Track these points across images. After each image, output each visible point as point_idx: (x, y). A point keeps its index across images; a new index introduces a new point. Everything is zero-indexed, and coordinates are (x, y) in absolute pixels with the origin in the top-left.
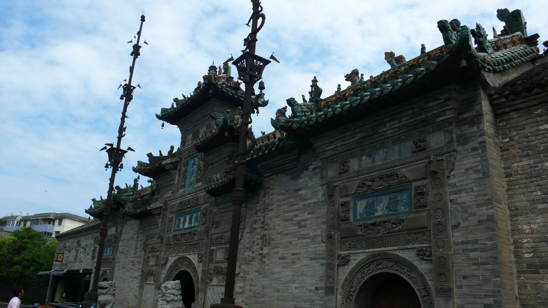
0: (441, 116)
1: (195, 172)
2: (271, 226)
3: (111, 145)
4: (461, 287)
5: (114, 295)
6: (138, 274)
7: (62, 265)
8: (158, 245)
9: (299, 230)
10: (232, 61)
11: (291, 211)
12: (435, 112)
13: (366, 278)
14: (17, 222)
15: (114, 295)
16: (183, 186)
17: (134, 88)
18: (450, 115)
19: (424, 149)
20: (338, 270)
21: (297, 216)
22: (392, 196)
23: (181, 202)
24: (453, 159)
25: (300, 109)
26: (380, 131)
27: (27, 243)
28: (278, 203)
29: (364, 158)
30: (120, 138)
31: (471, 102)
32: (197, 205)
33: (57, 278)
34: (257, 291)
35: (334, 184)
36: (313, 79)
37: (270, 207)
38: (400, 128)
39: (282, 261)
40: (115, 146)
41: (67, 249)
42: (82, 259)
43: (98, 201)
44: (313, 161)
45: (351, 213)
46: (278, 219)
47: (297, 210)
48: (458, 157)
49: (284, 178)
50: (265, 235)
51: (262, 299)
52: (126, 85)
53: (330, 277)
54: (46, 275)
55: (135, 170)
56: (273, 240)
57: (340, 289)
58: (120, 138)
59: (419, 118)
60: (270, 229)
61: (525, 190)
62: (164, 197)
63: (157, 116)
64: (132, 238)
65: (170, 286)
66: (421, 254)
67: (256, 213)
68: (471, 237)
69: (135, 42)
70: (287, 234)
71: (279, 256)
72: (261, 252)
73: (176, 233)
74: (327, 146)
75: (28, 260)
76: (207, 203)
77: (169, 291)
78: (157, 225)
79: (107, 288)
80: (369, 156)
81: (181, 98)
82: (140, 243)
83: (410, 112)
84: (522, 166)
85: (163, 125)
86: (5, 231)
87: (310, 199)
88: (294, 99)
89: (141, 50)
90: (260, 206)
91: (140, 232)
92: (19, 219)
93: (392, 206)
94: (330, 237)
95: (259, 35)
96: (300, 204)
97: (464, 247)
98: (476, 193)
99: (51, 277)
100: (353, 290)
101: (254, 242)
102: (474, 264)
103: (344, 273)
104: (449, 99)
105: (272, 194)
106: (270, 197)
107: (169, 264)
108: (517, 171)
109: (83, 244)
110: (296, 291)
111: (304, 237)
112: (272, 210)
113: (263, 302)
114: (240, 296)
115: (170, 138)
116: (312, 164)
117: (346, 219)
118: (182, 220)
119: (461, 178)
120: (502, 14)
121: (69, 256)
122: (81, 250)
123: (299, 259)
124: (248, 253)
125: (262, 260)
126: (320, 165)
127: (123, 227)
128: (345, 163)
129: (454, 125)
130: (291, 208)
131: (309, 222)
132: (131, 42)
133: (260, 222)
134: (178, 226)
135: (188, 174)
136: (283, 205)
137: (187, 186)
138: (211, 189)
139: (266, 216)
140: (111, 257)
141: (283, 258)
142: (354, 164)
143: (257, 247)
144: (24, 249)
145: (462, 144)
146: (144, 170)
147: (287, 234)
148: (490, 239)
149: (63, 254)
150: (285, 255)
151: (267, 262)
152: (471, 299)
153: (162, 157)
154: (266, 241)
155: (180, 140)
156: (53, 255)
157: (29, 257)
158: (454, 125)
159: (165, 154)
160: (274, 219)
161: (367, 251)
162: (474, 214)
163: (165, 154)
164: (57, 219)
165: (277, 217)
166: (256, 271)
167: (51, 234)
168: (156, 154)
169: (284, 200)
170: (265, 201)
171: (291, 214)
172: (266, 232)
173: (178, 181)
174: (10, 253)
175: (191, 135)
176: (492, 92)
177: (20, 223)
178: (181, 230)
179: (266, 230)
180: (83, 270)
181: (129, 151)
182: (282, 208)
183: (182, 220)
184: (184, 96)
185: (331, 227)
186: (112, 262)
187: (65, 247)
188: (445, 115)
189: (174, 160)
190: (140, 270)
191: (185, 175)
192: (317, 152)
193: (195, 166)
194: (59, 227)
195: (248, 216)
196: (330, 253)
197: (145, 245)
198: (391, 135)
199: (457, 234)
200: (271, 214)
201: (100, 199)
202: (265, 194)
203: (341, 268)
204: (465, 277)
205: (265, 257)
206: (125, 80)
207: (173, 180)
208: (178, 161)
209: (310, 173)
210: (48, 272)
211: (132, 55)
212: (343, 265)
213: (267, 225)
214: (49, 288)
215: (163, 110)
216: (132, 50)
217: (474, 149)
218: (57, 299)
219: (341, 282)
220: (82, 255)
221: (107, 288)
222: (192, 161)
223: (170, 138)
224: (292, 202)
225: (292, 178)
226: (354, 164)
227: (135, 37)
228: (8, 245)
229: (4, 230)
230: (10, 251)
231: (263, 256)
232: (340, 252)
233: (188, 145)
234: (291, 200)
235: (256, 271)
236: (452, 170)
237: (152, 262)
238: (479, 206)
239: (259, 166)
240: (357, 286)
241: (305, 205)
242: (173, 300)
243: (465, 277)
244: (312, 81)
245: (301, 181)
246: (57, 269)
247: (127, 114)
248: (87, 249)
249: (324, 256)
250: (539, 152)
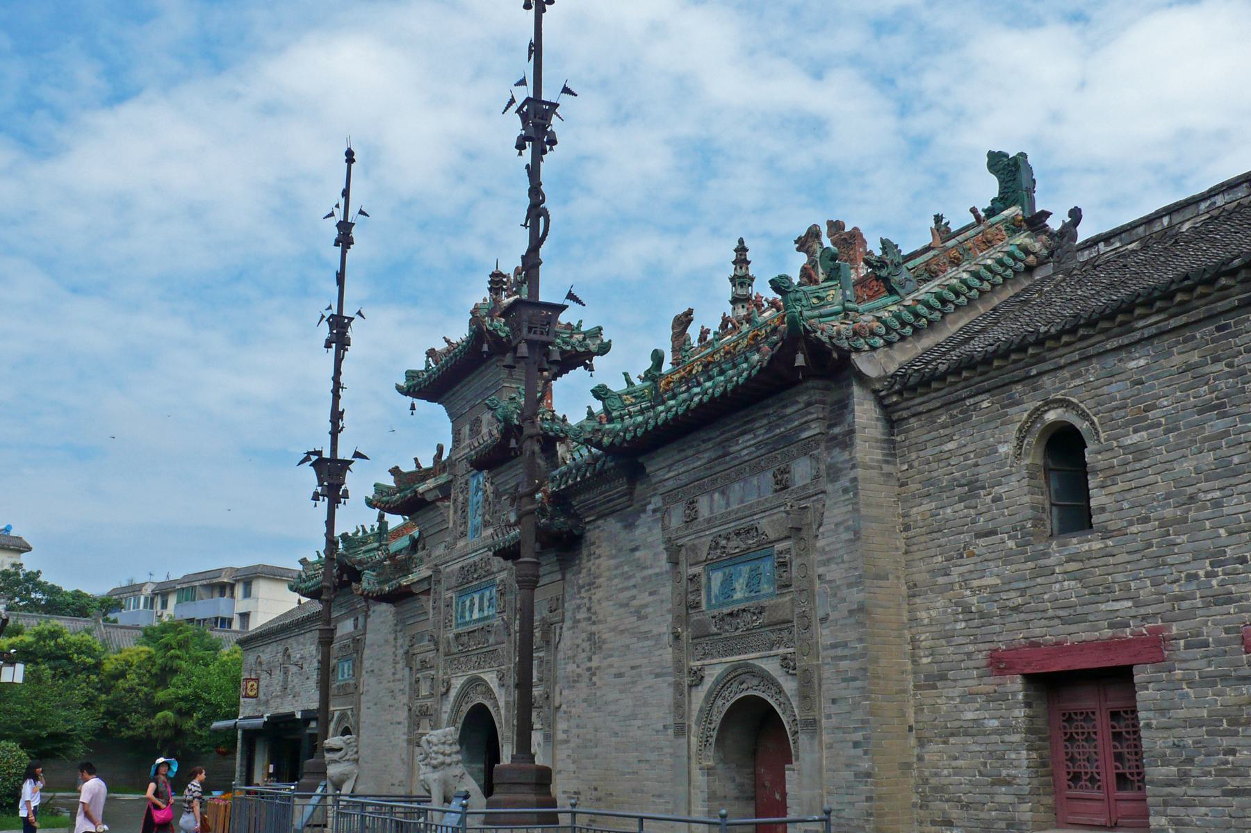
0: (805, 430)
2: (601, 617)
3: (319, 453)
4: (829, 717)
5: (356, 761)
6: (403, 715)
7: (259, 704)
8: (431, 655)
9: (639, 623)
10: (514, 107)
11: (627, 589)
12: (796, 423)
13: (728, 705)
14: (146, 599)
15: (356, 761)
16: (463, 534)
17: (351, 319)
18: (815, 429)
19: (786, 487)
20: (690, 695)
21: (634, 598)
22: (753, 565)
23: (463, 567)
24: (820, 506)
25: (618, 404)
26: (732, 449)
27: (178, 657)
28: (607, 574)
29: (716, 496)
30: (335, 432)
31: (842, 407)
32: (489, 573)
33: (251, 736)
34: (588, 737)
35: (680, 542)
36: (736, 244)
38: (757, 446)
39: (618, 680)
40: (327, 454)
41: (264, 667)
42: (297, 689)
43: (313, 564)
45: (703, 592)
47: (634, 586)
48: (828, 503)
50: (592, 634)
51: (594, 750)
52: (332, 316)
53: (679, 707)
54: (228, 729)
55: (370, 503)
56: (604, 642)
57: (693, 726)
58: (335, 432)
59: (778, 431)
60: (600, 622)
61: (924, 554)
62: (433, 555)
63: (399, 388)
64: (386, 641)
65: (434, 740)
66: (787, 664)
67: (579, 592)
68: (841, 637)
69: (339, 216)
70: (622, 632)
71: (614, 671)
72: (589, 664)
73: (460, 630)
74: (667, 470)
75: (185, 699)
77: (435, 748)
78: (426, 613)
79: (341, 749)
81: (441, 346)
82: (401, 652)
83: (765, 421)
84: (923, 513)
85: (413, 407)
86: (122, 627)
87: (652, 567)
88: (604, 387)
89: (355, 232)
90: (583, 578)
91: (399, 628)
92: (149, 591)
93: (753, 583)
94: (677, 637)
95: (544, 250)
96: (639, 575)
97: (833, 652)
98: (847, 565)
99: (240, 732)
100: (712, 726)
101: (578, 646)
102: (844, 680)
103: (698, 697)
104: (809, 404)
105: (599, 557)
106: (597, 562)
107: (453, 693)
108: (916, 521)
109: (296, 656)
110: (639, 733)
111: (645, 636)
113: (596, 756)
114: (564, 746)
115: (428, 434)
117: (697, 606)
118: (468, 603)
119: (830, 540)
120: (997, 162)
121: (271, 683)
122: (293, 669)
123: (640, 676)
124: (571, 667)
125: (591, 679)
126: (660, 504)
127: (367, 616)
128: (691, 504)
129: (823, 446)
131: (650, 610)
132: (332, 215)
133: (585, 609)
134: (463, 617)
135: (469, 509)
136: (615, 576)
140: (352, 682)
141: (620, 675)
142: (704, 507)
143: (584, 655)
144: (174, 671)
145: (832, 481)
146: (387, 502)
147: (622, 632)
148: (861, 640)
149: (257, 680)
150: (622, 670)
151: (598, 683)
152: (840, 735)
153: (422, 475)
154: (595, 643)
156: (236, 682)
157: (188, 691)
158: (823, 446)
159: (427, 463)
160: (604, 604)
161: (724, 660)
162: (844, 600)
163: (427, 463)
164: (238, 581)
166: (585, 701)
167: (230, 621)
168: (408, 467)
169: (616, 568)
172: (594, 628)
174: (145, 685)
175: (468, 427)
176: (877, 386)
177: (152, 599)
178: (466, 623)
179: (594, 623)
180: (303, 712)
181: (357, 460)
182: (615, 581)
183: (468, 603)
184: (448, 341)
185: (678, 619)
186: (352, 692)
187: (260, 663)
188: (809, 428)
189: (443, 478)
190: (406, 708)
192: (654, 481)
194: (247, 601)
195: (567, 597)
196: (679, 667)
197: (409, 656)
198: (747, 458)
199: (826, 632)
200: (599, 594)
201: (317, 558)
202: (590, 555)
203: (693, 689)
204: (834, 701)
205: (594, 674)
206: (330, 308)
208: (451, 481)
210: (230, 723)
211: (337, 244)
212: (697, 685)
213: (595, 613)
214: (238, 756)
215: (411, 375)
216: (335, 233)
217: (845, 491)
218: (258, 777)
219: (695, 714)
220: (296, 680)
221: (341, 749)
223: (428, 434)
225: (625, 527)
227: (337, 206)
228: (139, 667)
229: (120, 623)
230: (145, 680)
231: (592, 672)
232: (692, 664)
234: (626, 568)
235: (585, 701)
236: (820, 525)
237: (424, 690)
238: (850, 586)
240: (717, 719)
241: (644, 578)
242: (443, 763)
243: (834, 701)
244: (736, 250)
246: (250, 713)
247: (342, 379)
248: (305, 666)
249: (670, 670)
250: (942, 490)
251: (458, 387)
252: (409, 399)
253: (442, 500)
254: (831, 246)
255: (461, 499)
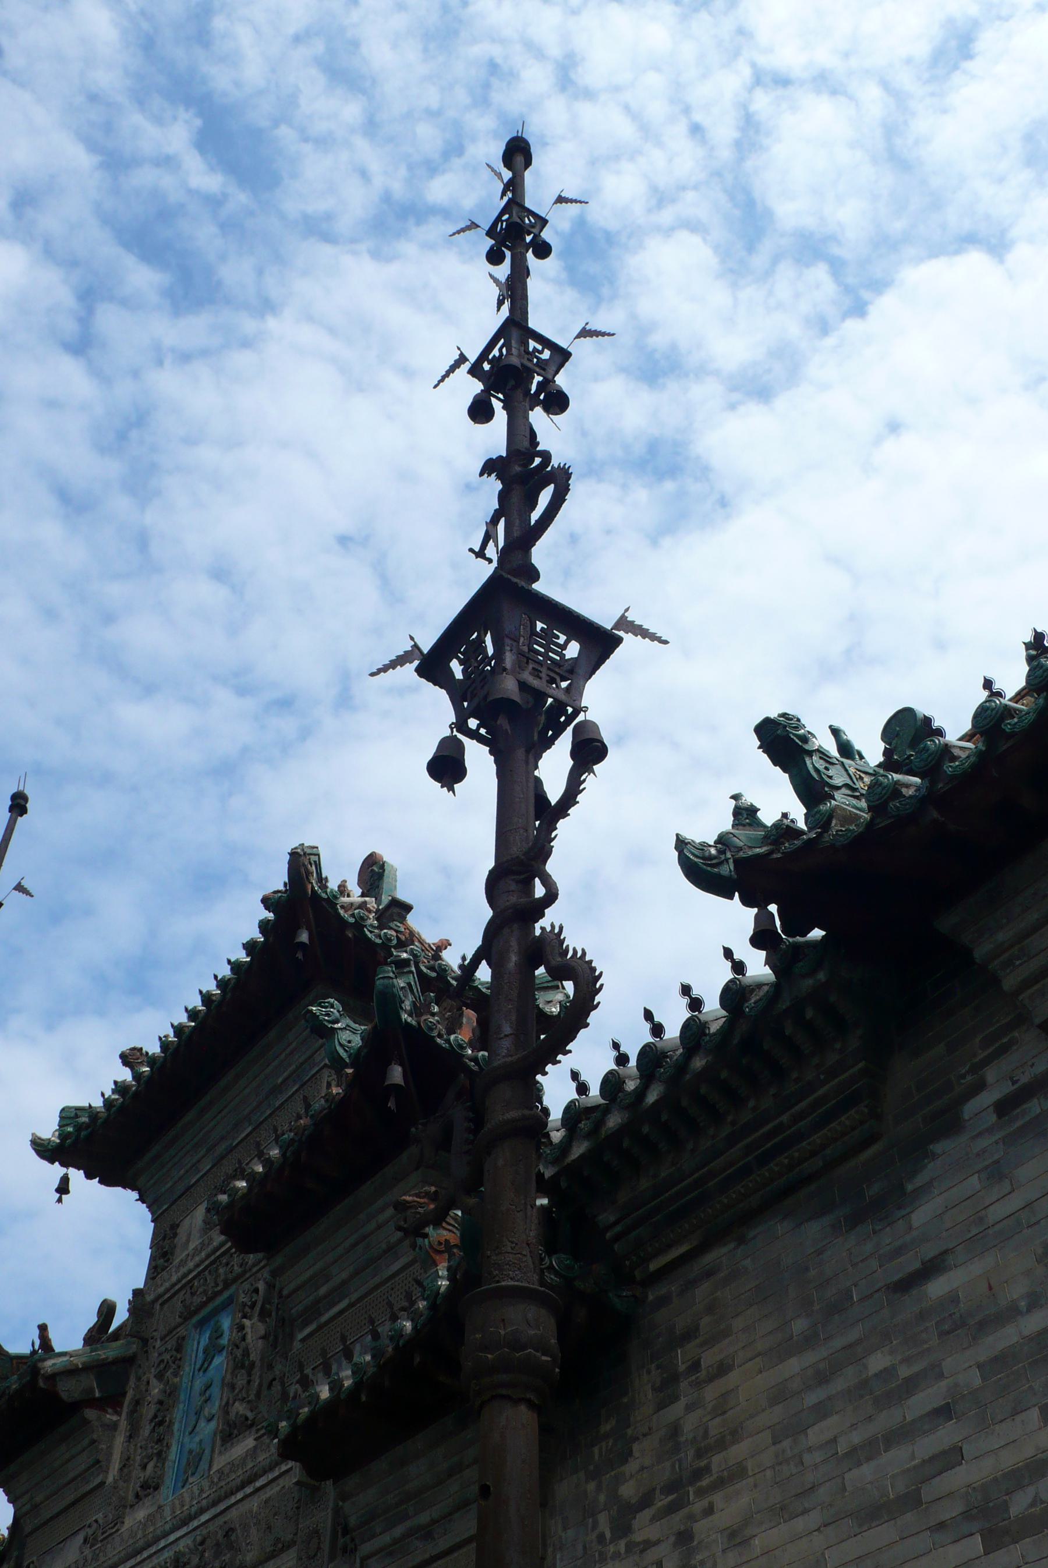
1: (215, 1391)
10: (467, 366)
21: (952, 1457)
37: (717, 1462)
44: (986, 1062)
46: (800, 1524)
47: (944, 1412)
49: (790, 1241)
67: (622, 1528)
76: (286, 1547)
85: (63, 1188)
90: (642, 1468)
96: (962, 1367)
105: (723, 1369)
106: (711, 1393)
112: (738, 1472)
116: (980, 1086)
130: (888, 1419)
135: (178, 1414)
136: (821, 1411)
137: (169, 1481)
138: (312, 1418)
139: (700, 1527)
155: (148, 1253)
165: (782, 1512)
169: (822, 1378)
170: (675, 1430)
171: (898, 1459)
173: (126, 1463)
182: (816, 1434)
191: (160, 1422)
192: (1009, 983)
193: (218, 1360)
200: (730, 1507)
202: (673, 1379)
207: (98, 1465)
209: (985, 1142)
222: (205, 1340)
224: (888, 1373)
225: (855, 1220)
233: (183, 1263)
234: (877, 1362)
239: (607, 1217)
241: (1000, 1360)
245: (921, 1216)
251: (190, 1116)
252: (57, 1171)
253: (100, 1404)
254: (556, 1114)
255: (156, 1390)
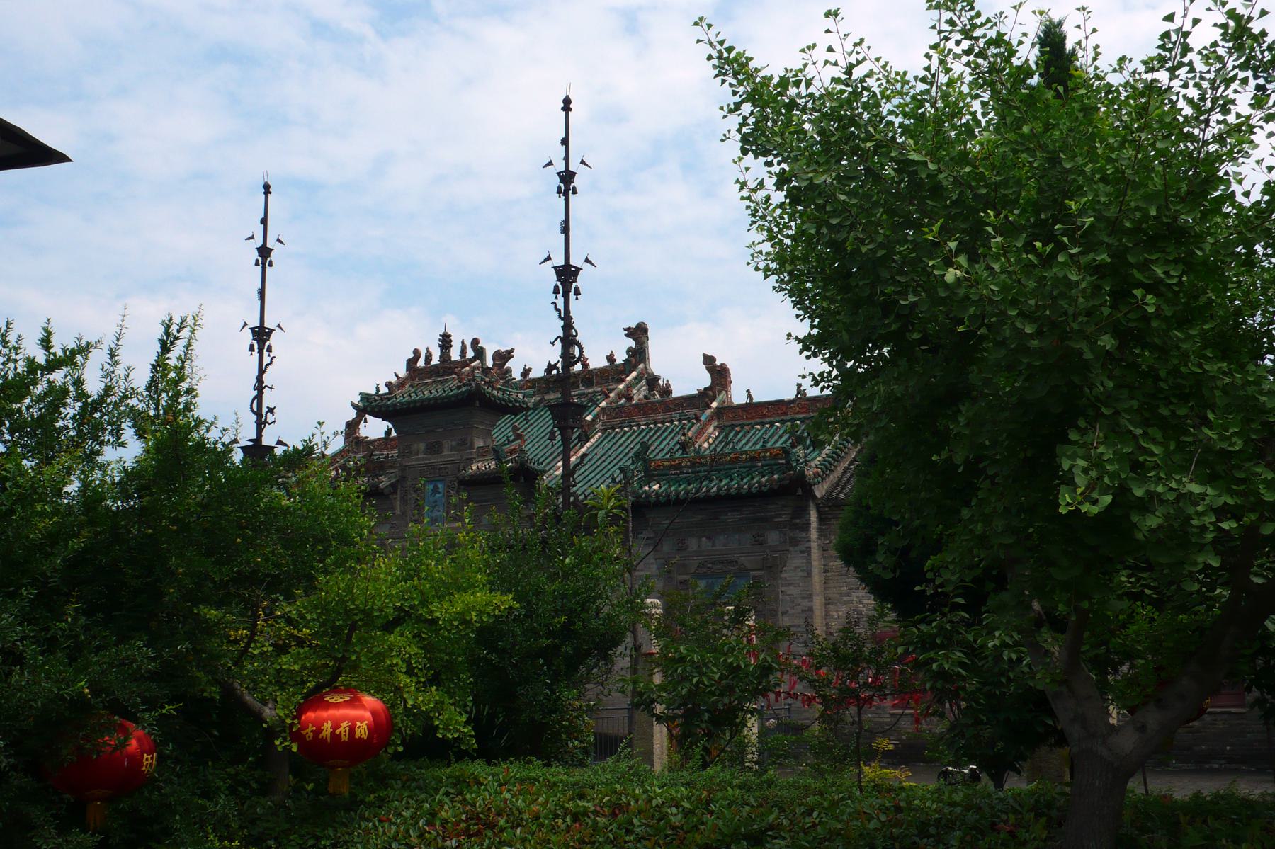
18: (784, 519)
80: (709, 538)
226: (693, 544)
238: (803, 598)
